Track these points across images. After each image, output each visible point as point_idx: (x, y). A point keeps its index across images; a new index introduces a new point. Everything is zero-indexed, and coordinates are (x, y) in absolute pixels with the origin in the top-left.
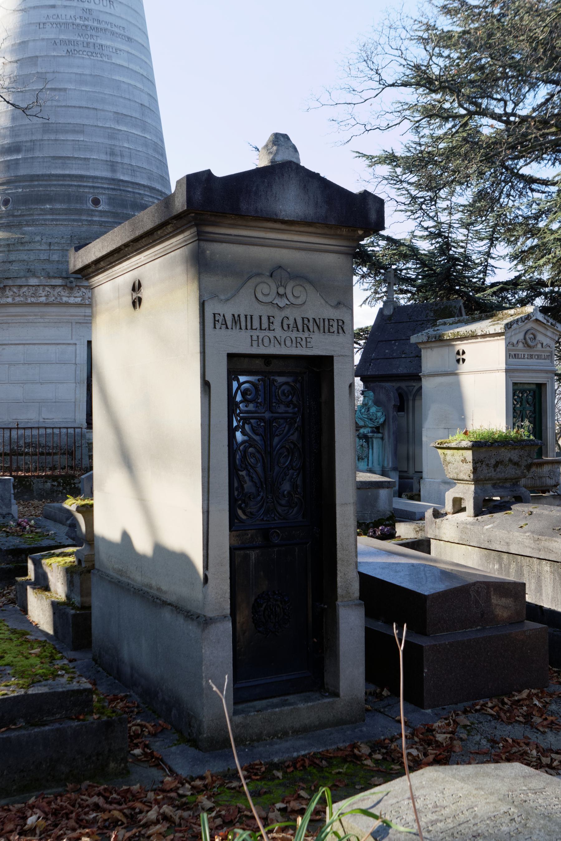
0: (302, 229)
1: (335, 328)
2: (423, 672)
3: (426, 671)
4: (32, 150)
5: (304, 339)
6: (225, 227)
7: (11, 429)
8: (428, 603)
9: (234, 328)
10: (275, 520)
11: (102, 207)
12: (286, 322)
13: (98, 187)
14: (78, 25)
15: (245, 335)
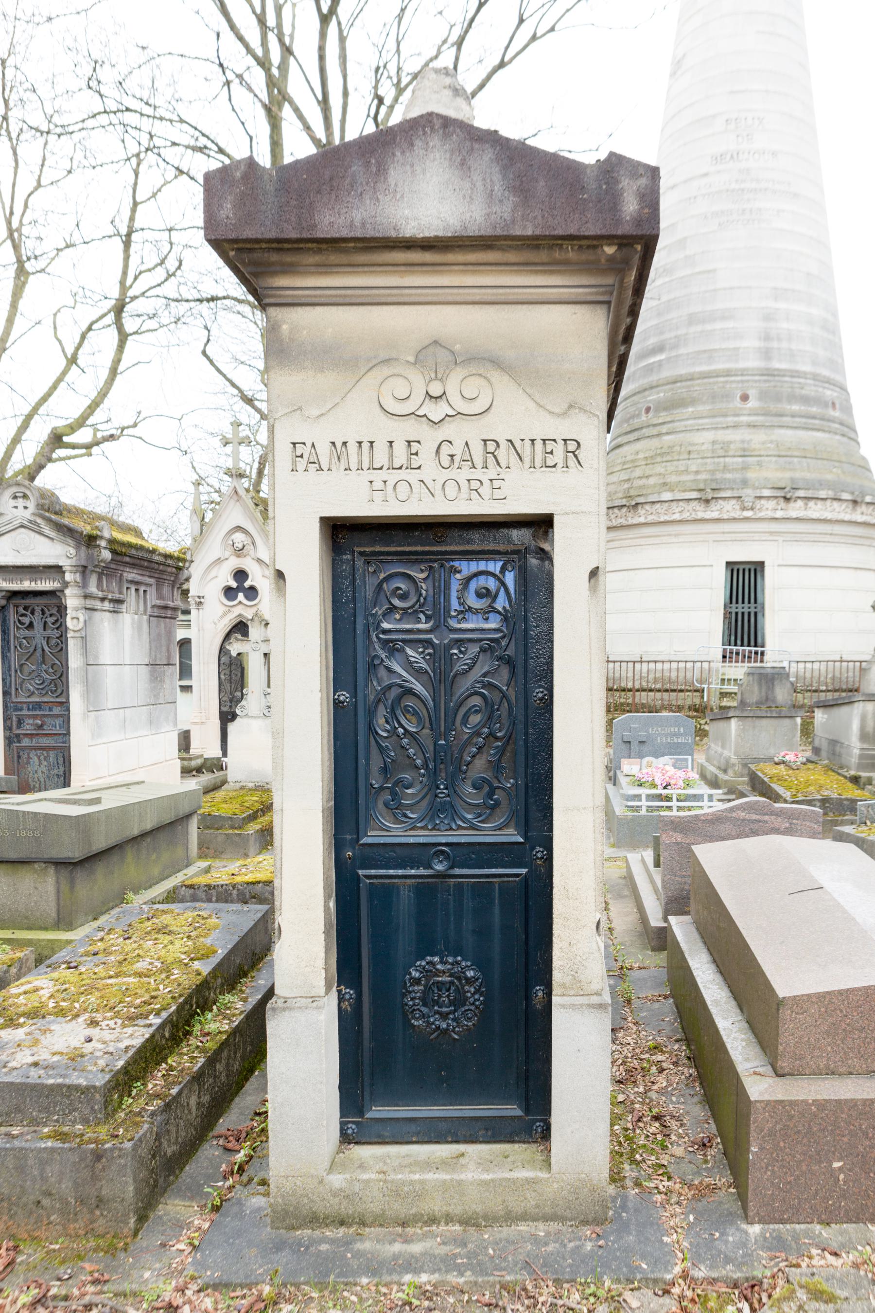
0: (472, 257)
1: (558, 457)
2: (748, 1150)
3: (754, 1149)
4: (675, 346)
5: (487, 483)
6: (312, 273)
7: (634, 662)
8: (785, 1013)
9: (333, 468)
10: (451, 829)
11: (752, 403)
12: (446, 450)
13: (748, 381)
14: (733, 191)
15: (358, 481)
